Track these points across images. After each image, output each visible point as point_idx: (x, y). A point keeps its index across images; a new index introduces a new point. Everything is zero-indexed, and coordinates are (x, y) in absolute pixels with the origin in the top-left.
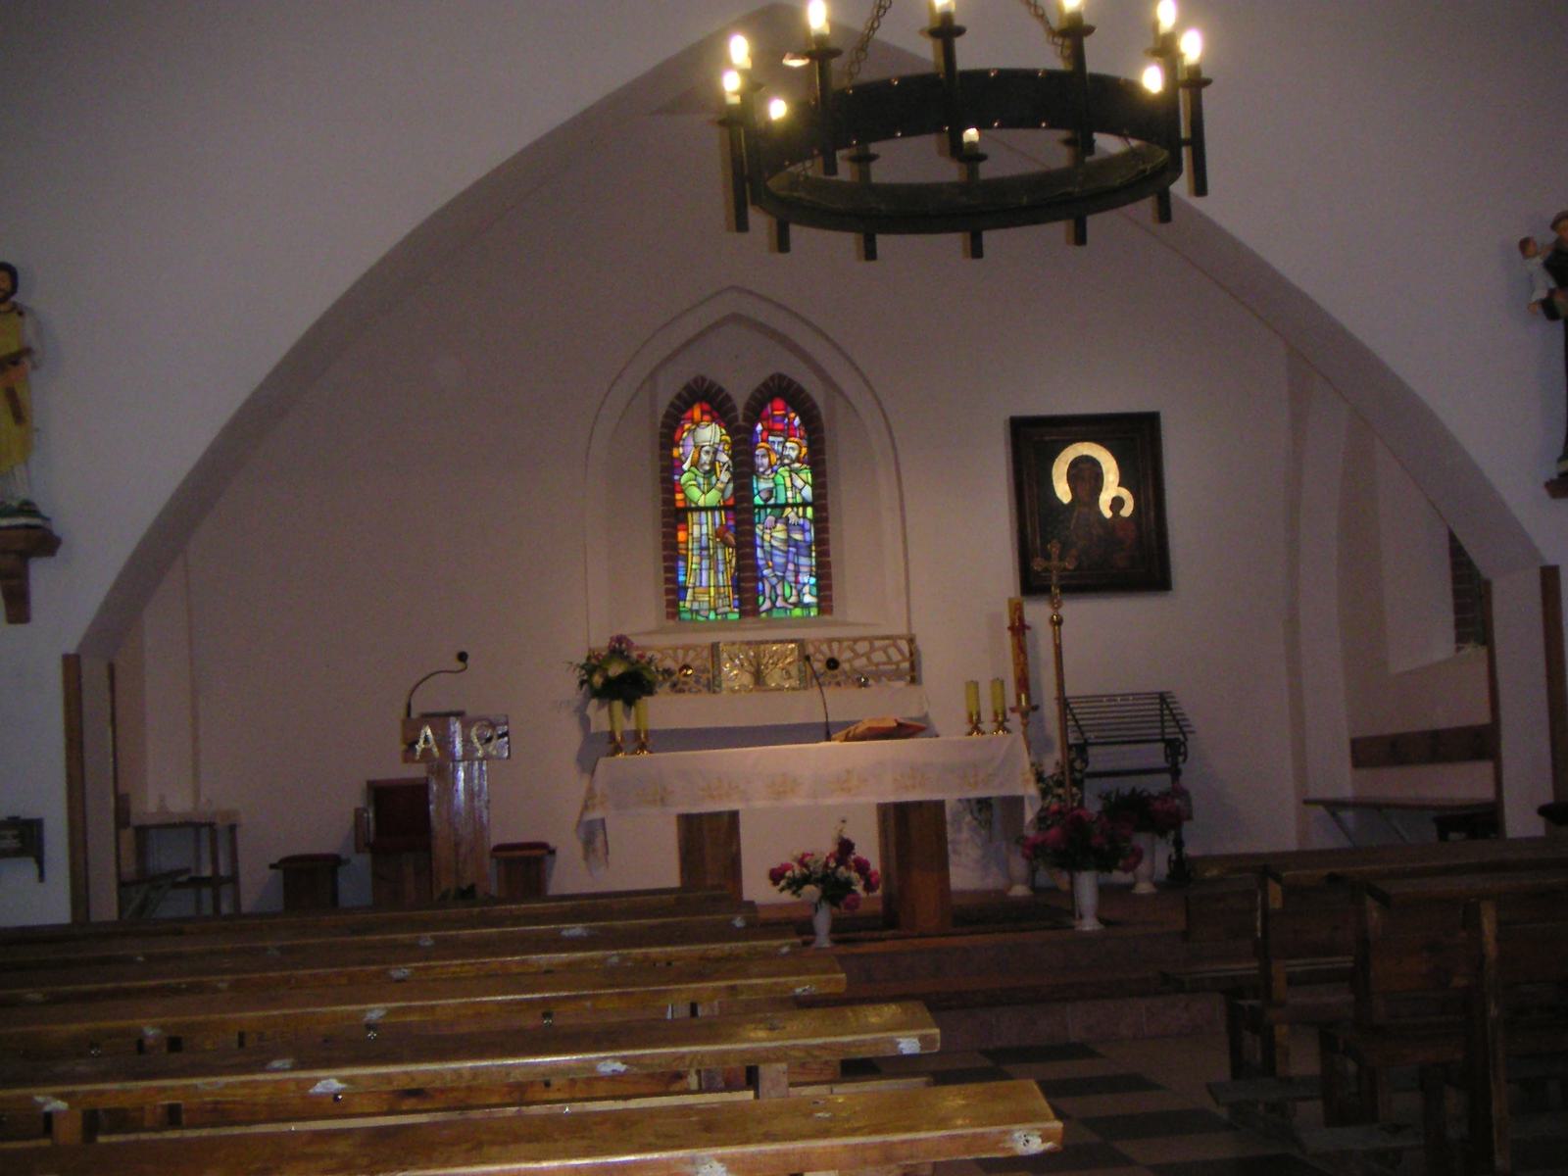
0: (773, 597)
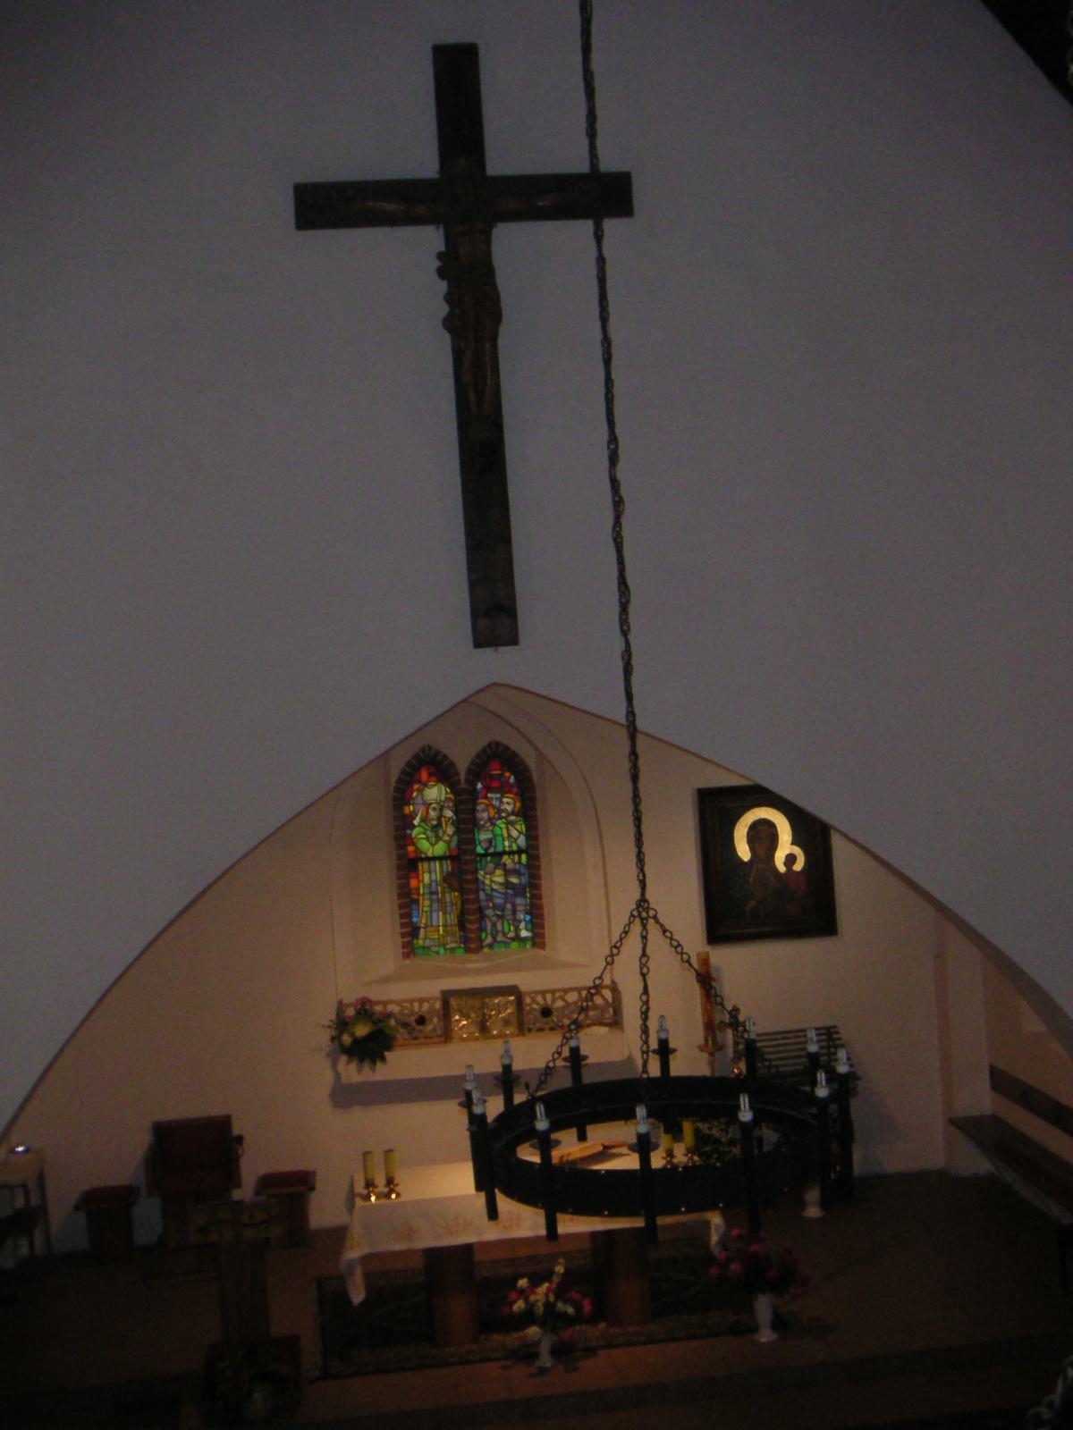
0: (494, 933)
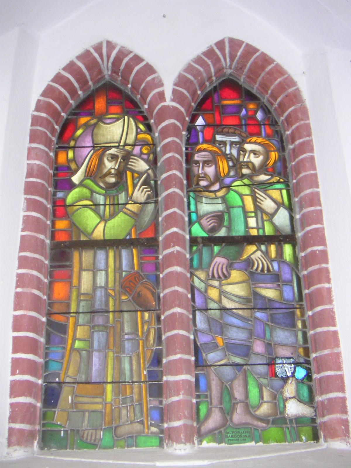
0: (226, 405)
